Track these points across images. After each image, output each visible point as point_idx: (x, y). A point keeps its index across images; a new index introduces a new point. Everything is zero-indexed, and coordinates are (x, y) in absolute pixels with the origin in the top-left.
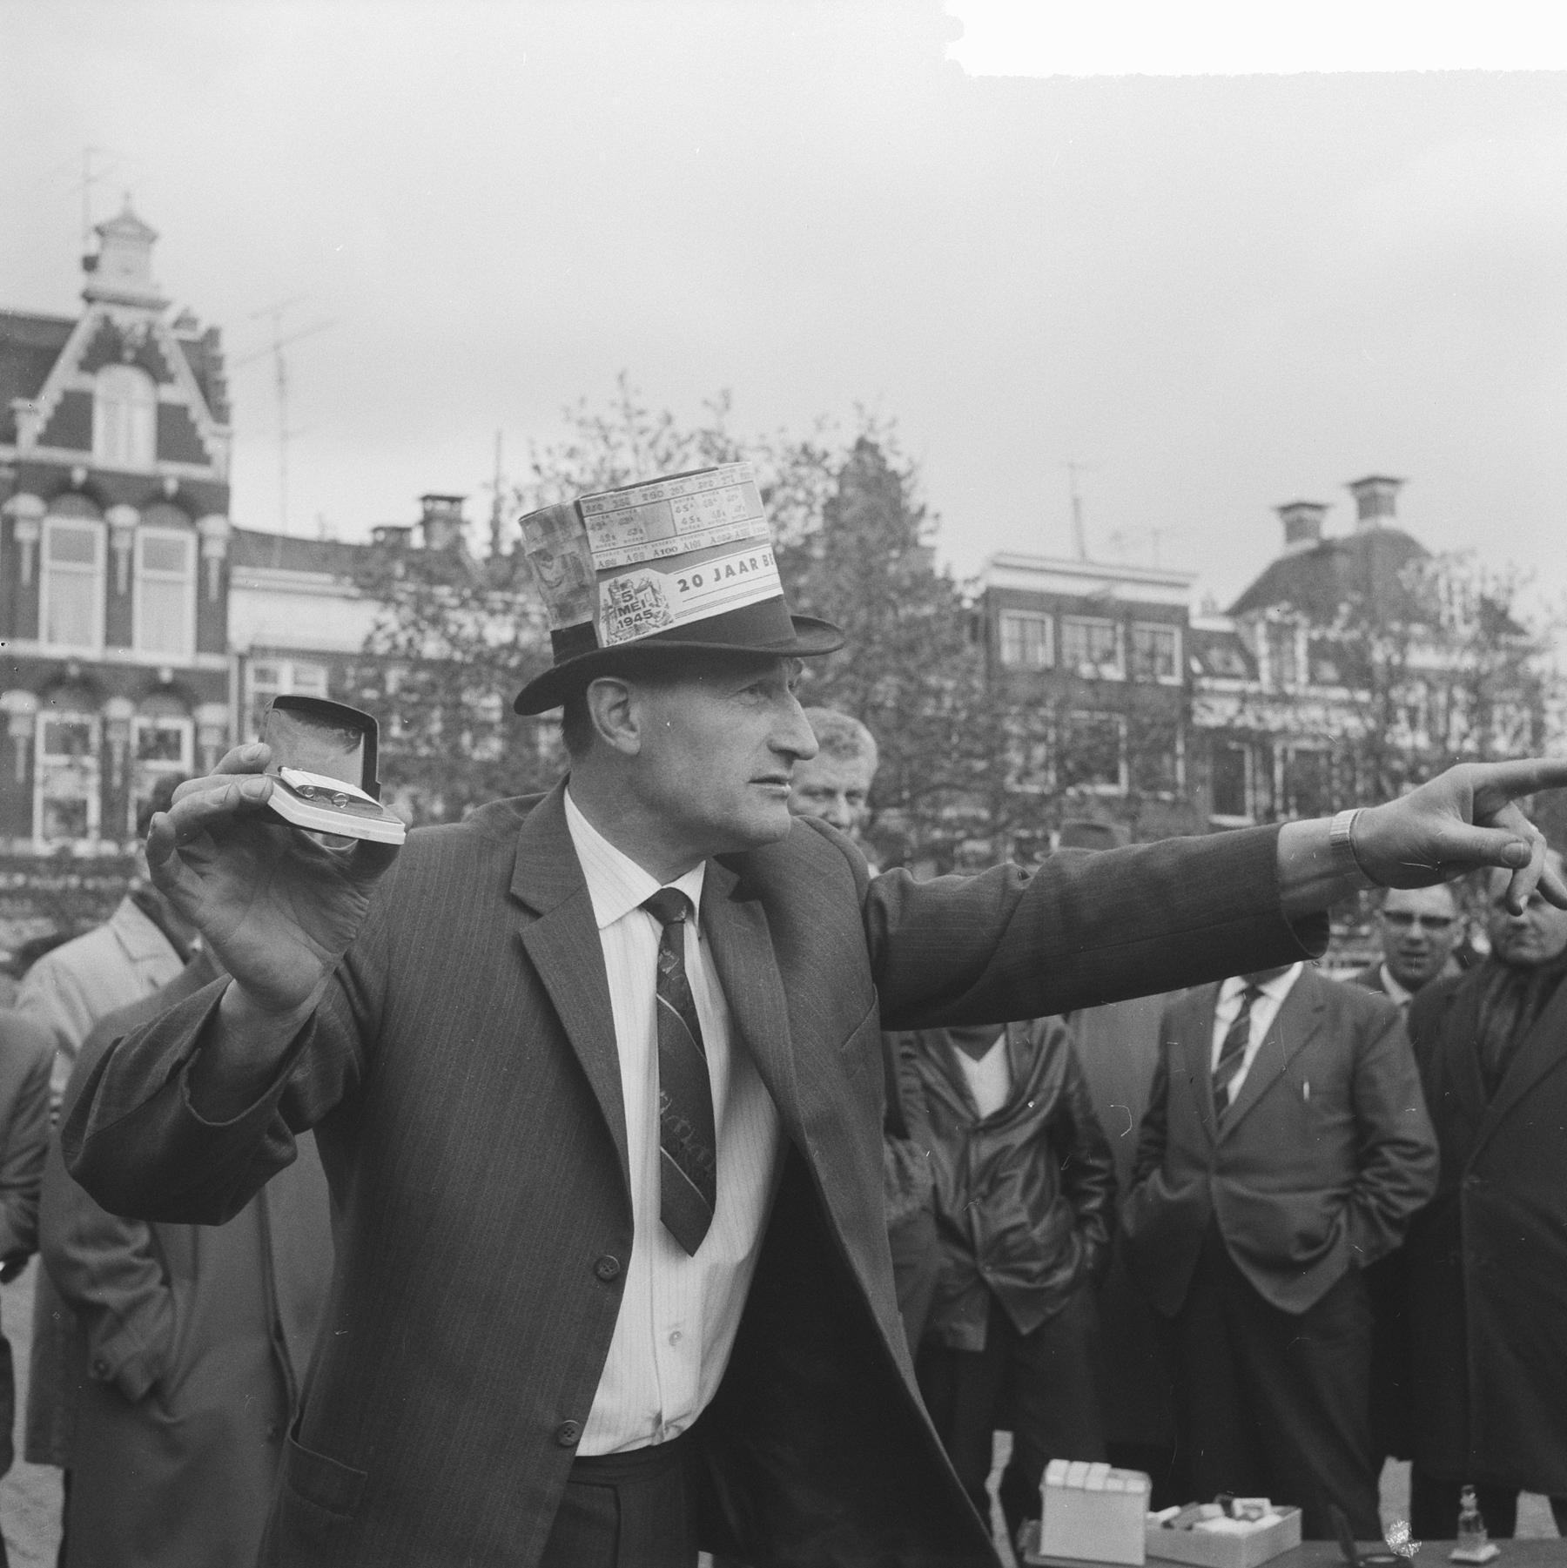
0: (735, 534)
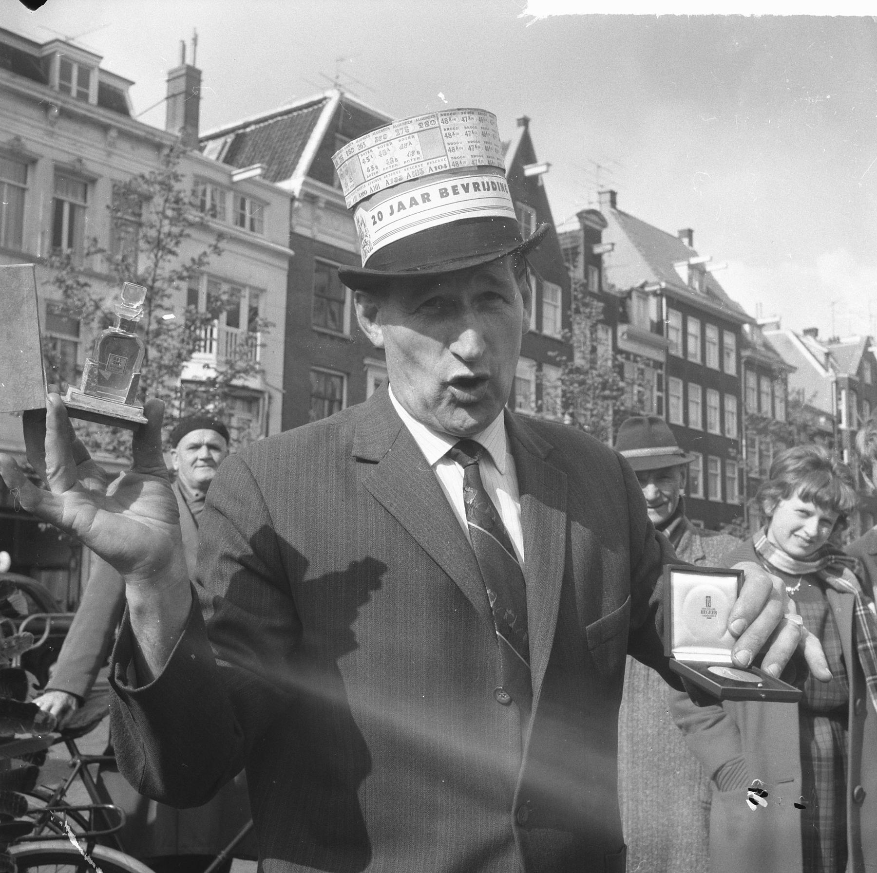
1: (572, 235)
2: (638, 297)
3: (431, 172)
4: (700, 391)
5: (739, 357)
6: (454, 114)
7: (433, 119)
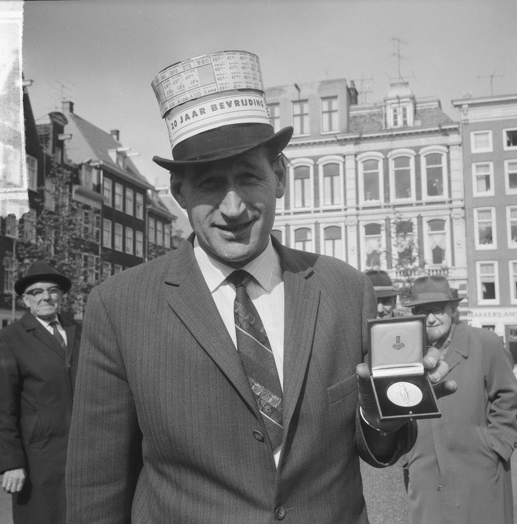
0: (190, 96)
1: (45, 127)
2: (86, 169)
3: (206, 94)
4: (121, 229)
5: (145, 209)
6: (222, 55)
7: (207, 59)
